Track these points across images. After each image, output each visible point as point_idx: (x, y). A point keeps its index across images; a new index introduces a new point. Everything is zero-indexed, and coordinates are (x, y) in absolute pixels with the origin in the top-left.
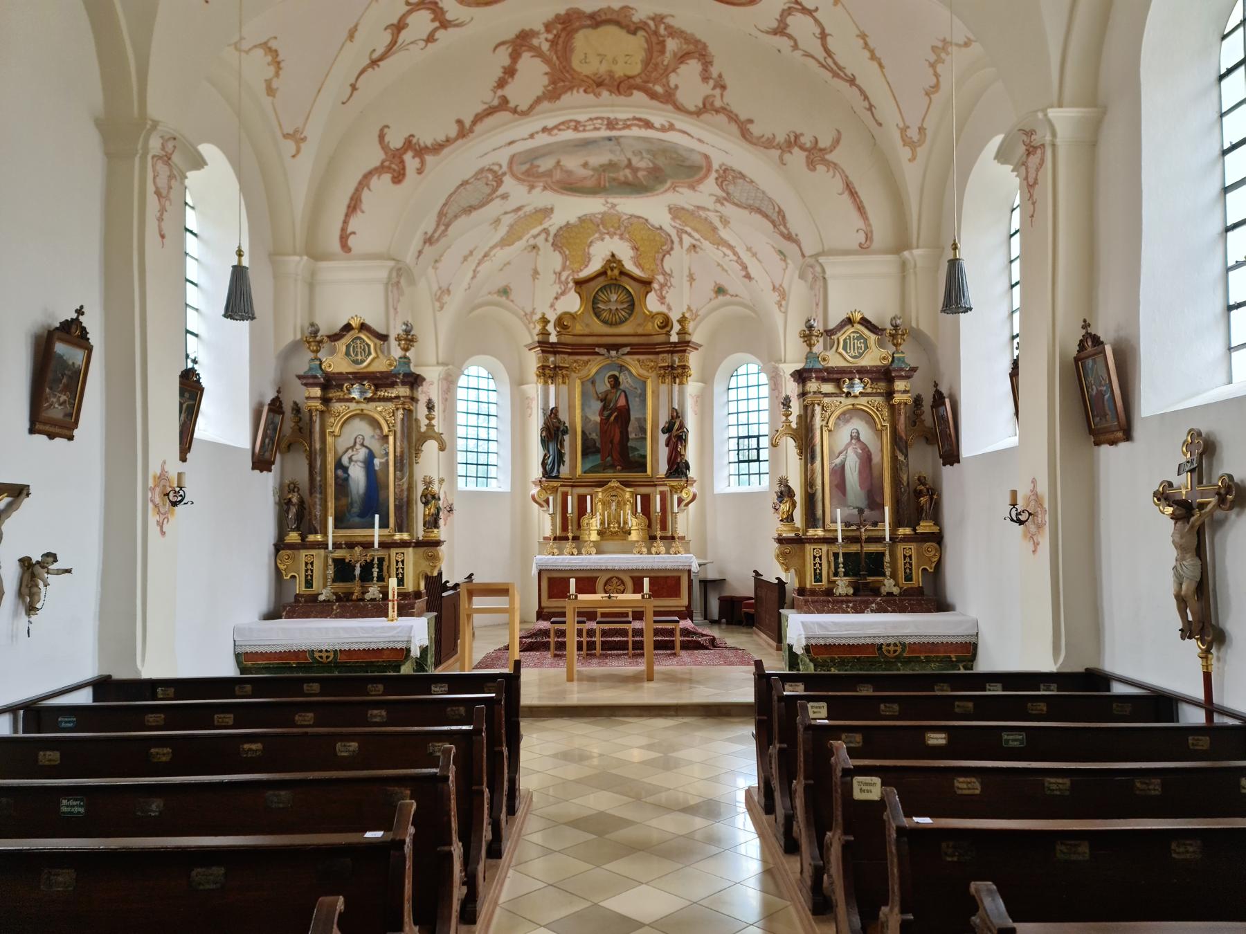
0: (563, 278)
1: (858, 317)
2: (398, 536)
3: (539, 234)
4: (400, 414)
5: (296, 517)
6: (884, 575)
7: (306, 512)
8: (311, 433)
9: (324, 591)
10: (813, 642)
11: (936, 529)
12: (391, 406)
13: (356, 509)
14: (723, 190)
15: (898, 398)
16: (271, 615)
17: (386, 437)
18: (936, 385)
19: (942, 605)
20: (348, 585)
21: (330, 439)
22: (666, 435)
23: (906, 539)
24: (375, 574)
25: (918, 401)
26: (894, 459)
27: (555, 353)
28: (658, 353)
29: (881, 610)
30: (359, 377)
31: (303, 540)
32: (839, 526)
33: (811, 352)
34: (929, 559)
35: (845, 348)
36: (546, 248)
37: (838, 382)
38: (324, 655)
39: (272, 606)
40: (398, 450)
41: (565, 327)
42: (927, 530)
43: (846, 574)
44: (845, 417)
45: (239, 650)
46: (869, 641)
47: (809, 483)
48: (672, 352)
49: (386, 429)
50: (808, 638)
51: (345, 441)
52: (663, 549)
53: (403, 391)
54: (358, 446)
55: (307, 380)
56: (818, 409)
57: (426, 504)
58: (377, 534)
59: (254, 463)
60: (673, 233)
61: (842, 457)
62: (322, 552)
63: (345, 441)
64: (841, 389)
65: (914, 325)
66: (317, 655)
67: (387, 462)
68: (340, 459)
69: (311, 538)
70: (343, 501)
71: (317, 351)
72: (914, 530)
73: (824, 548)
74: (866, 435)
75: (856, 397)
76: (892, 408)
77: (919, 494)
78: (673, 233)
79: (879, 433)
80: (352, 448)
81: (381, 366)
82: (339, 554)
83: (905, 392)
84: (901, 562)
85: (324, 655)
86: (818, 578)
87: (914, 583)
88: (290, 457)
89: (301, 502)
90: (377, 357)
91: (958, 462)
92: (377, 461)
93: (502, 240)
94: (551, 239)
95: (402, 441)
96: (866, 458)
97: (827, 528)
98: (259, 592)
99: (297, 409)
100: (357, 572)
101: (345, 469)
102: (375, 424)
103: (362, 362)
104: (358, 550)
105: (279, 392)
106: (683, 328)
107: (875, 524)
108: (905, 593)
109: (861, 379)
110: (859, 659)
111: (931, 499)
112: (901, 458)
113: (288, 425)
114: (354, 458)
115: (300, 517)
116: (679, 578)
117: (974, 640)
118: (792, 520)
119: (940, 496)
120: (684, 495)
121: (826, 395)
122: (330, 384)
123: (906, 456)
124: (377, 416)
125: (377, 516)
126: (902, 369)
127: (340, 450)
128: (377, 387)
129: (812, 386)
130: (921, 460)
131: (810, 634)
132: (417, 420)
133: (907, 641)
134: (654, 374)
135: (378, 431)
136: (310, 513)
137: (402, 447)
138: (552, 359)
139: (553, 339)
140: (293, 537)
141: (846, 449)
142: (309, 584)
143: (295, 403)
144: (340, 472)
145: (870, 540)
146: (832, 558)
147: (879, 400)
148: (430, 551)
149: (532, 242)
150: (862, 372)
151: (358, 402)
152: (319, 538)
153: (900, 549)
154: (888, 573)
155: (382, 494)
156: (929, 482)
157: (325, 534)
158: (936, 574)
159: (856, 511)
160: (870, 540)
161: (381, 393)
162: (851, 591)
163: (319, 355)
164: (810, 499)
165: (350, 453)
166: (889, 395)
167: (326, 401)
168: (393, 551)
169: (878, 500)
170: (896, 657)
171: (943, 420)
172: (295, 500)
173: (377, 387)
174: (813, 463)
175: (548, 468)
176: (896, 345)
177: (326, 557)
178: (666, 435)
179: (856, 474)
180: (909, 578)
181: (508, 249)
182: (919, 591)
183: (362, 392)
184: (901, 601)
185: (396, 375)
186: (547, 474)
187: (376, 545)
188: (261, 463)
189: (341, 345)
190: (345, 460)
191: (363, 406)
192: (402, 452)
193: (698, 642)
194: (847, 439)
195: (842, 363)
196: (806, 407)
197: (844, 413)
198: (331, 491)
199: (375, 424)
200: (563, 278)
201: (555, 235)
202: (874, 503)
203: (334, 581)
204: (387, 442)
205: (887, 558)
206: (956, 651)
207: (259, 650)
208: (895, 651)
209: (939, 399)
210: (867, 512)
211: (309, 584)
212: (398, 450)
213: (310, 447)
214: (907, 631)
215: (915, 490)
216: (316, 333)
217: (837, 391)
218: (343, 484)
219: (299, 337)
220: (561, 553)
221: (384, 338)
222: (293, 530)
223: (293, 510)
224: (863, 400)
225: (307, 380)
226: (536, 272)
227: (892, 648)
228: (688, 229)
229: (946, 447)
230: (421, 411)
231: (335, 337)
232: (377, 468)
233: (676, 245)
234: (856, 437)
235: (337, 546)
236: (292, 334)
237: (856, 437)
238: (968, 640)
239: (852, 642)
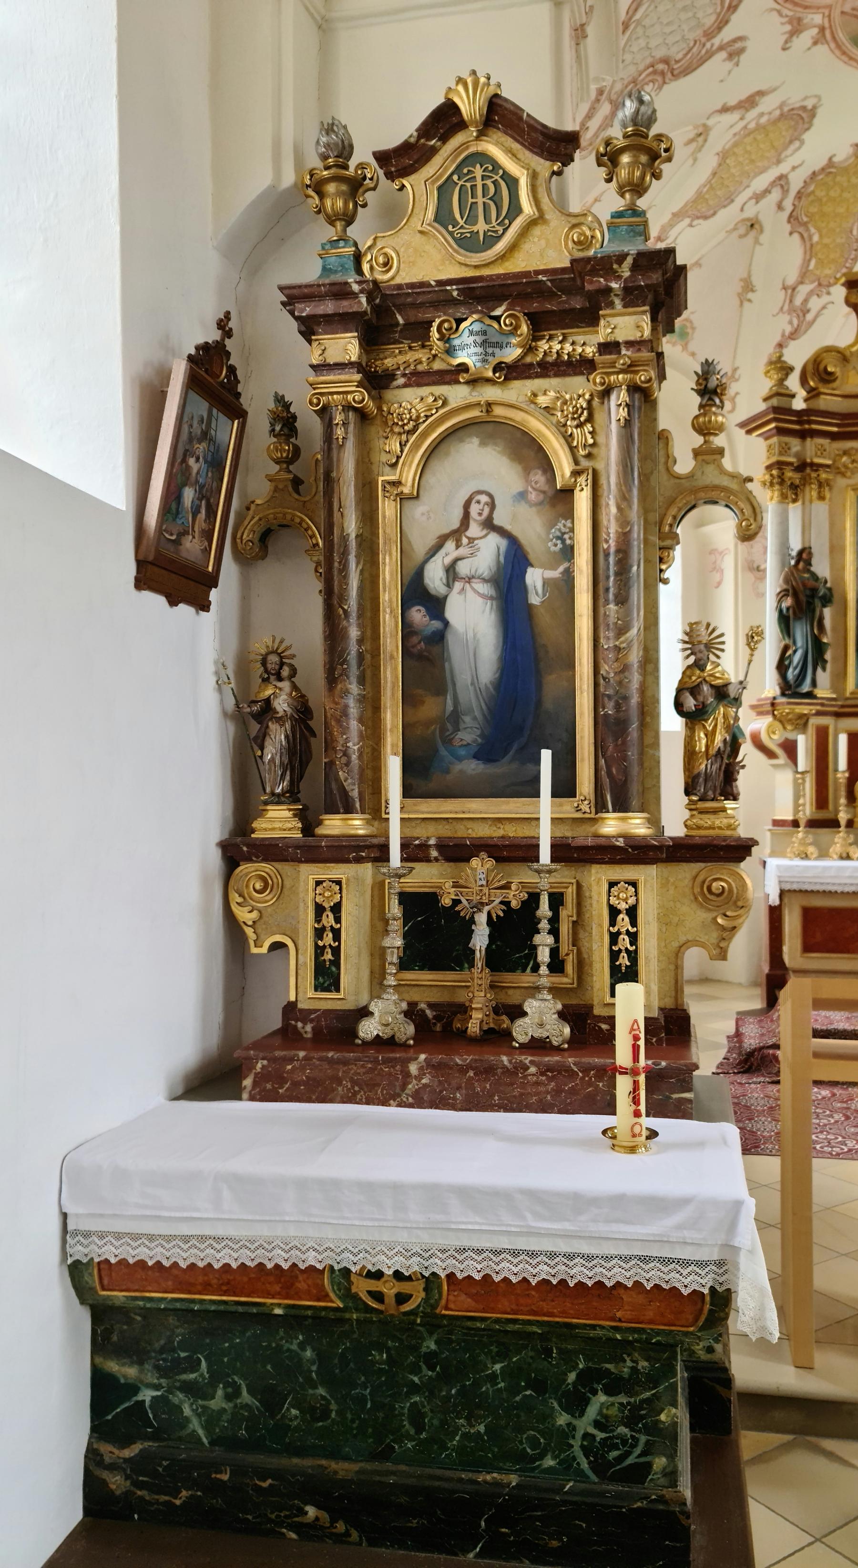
0: (798, 301)
1: (470, 107)
2: (612, 825)
3: (767, 191)
4: (617, 408)
5: (286, 758)
7: (317, 744)
8: (330, 482)
9: (376, 1007)
12: (579, 387)
13: (469, 734)
16: (212, 1080)
17: (567, 494)
20: (447, 978)
21: (387, 509)
24: (544, 955)
27: (803, 435)
30: (480, 294)
31: (308, 829)
36: (775, 223)
38: (390, 1290)
39: (214, 1040)
40: (611, 528)
41: (827, 377)
45: (78, 1252)
49: (564, 466)
51: (431, 516)
53: (626, 324)
54: (474, 530)
55: (312, 310)
57: (694, 717)
58: (545, 816)
59: (141, 564)
62: (366, 870)
63: (431, 516)
66: (361, 1287)
67: (569, 578)
68: (419, 573)
69: (334, 825)
70: (430, 708)
71: (349, 220)
80: (456, 534)
81: (546, 252)
82: (427, 876)
85: (390, 1290)
88: (269, 573)
89: (303, 712)
90: (538, 220)
92: (534, 577)
93: (699, 197)
94: (788, 205)
95: (624, 498)
98: (171, 1005)
99: (285, 421)
100: (480, 939)
101: (436, 606)
102: (528, 452)
103: (491, 239)
104: (480, 867)
105: (223, 325)
113: (257, 477)
114: (463, 568)
115: (298, 757)
122: (388, 319)
124: (536, 425)
125: (546, 756)
127: (420, 545)
128: (540, 324)
132: (664, 437)
135: (538, 477)
136: (329, 745)
137: (623, 520)
138: (795, 444)
139: (799, 404)
140: (278, 822)
142: (327, 975)
143: (279, 399)
144: (418, 615)
148: (721, 876)
149: (750, 212)
151: (474, 382)
152: (357, 825)
155: (552, 683)
157: (376, 810)
161: (551, 346)
163: (353, 231)
165: (450, 550)
167: (377, 381)
168: (598, 877)
172: (282, 705)
173: (540, 324)
175: (791, 674)
177: (379, 888)
181: (704, 226)
183: (487, 344)
185: (605, 265)
186: (789, 689)
187: (545, 855)
188: (170, 572)
189: (420, 187)
190: (434, 577)
191: (490, 393)
192: (624, 538)
198: (392, 673)
199: (528, 452)
200: (798, 301)
201: (799, 195)
203: (404, 965)
204: (569, 514)
207: (151, 1254)
208: (401, 1299)
211: (327, 975)
212: (611, 528)
213: (328, 534)
216: (345, 150)
218: (427, 653)
219: (289, 178)
220: (823, 854)
221: (558, 146)
222: (277, 799)
223: (278, 737)
225: (312, 310)
226: (748, 286)
230: (676, 402)
231: (400, 161)
232: (535, 600)
235: (414, 852)
236: (271, 162)
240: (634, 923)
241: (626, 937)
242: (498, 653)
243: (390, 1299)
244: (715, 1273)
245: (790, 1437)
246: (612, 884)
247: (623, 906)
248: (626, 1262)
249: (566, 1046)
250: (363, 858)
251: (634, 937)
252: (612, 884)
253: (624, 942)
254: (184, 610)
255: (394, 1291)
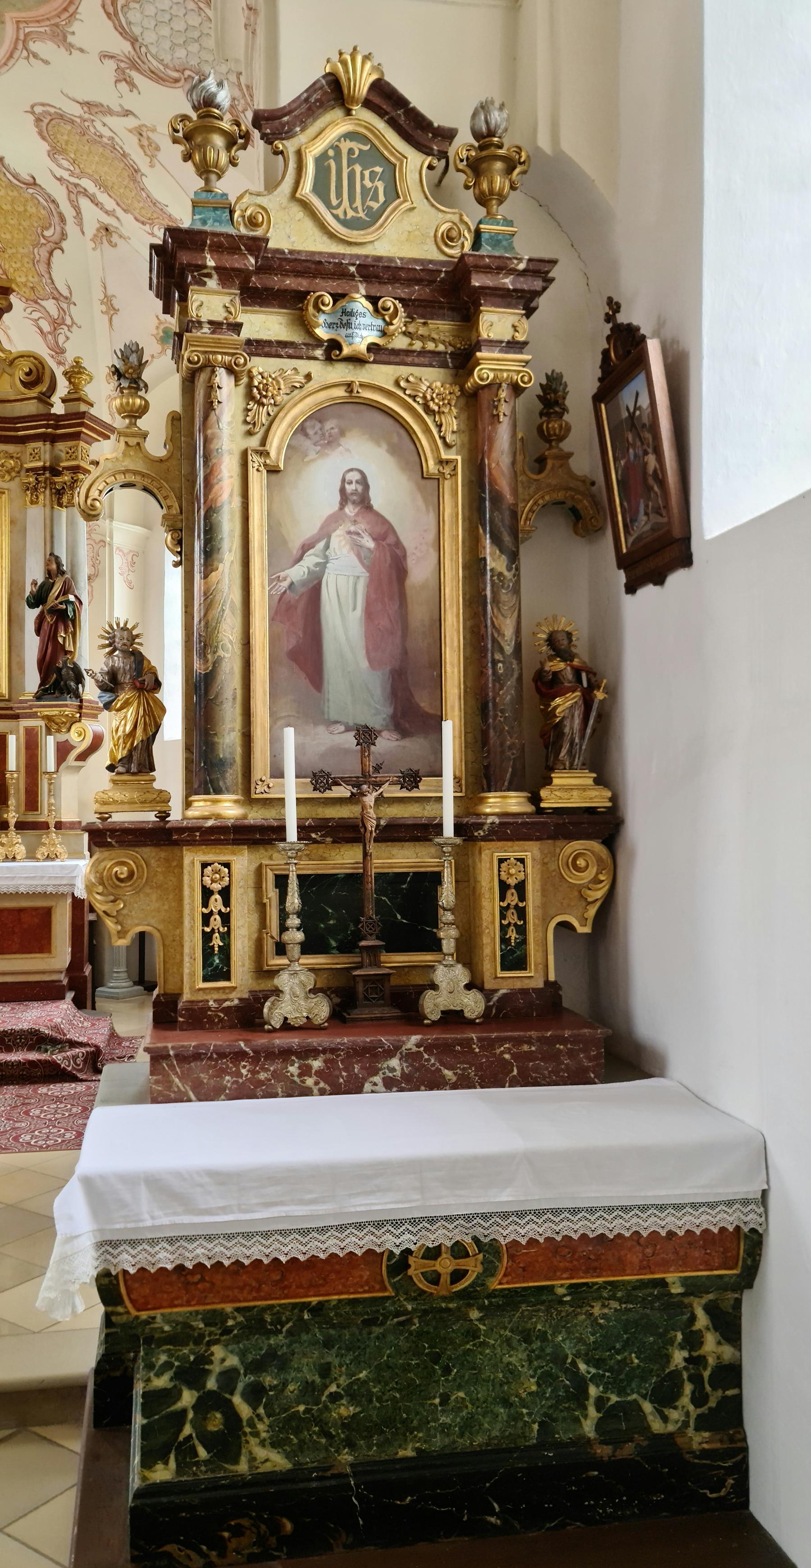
1: (362, 82)
6: (435, 945)
10: (127, 1262)
11: (599, 798)
14: (124, 33)
15: (490, 366)
18: (614, 306)
19: (621, 1057)
22: (37, 611)
23: (509, 830)
25: (552, 396)
26: (475, 567)
28: (24, 440)
29: (420, 1079)
32: (291, 789)
33: (208, 190)
34: (580, 892)
35: (321, 188)
37: (294, 302)
42: (575, 801)
43: (307, 948)
44: (320, 429)
46: (356, 1244)
47: (200, 641)
48: (53, 439)
50: (108, 1245)
52: (21, 850)
56: (229, 394)
60: (59, 193)
61: (310, 560)
64: (306, 326)
65: (544, 142)
72: (535, 799)
73: (243, 862)
74: (391, 491)
75: (356, 360)
76: (475, 403)
77: (548, 686)
78: (59, 193)
79: (429, 483)
83: (514, 346)
84: (490, 906)
86: (217, 967)
87: (531, 978)
91: (686, 560)
96: (390, 569)
97: (259, 791)
106: (75, 387)
107: (411, 779)
108: (505, 1012)
109: (373, 300)
110: (317, 1310)
111: (588, 702)
112: (495, 561)
116: (45, 916)
117: (752, 1220)
118: (148, 766)
119: (613, 692)
120: (73, 736)
121: (260, 347)
123: (514, 557)
126: (502, 267)
129: (210, 302)
130: (561, 582)
131: (119, 1227)
133: (505, 1234)
134: (14, 485)
141: (325, 533)
145: (394, 833)
146: (272, 893)
147: (432, 379)
150: (377, 274)
153: (488, 860)
154: (448, 945)
156: (581, 648)
158: (598, 941)
159: (349, 740)
160: (394, 833)
162: (322, 1009)
164: (201, 691)
166: (462, 360)
169: (424, 702)
170: (464, 1295)
171: (641, 428)
174: (209, 567)
176: (483, 200)
178: (37, 611)
179: (356, 617)
180: (514, 959)
182: (547, 1004)
184: (488, 1045)
187: (292, 834)
193: (53, 1065)
194: (330, 502)
195: (310, 242)
196: (189, 382)
197: (319, 415)
202: (414, 717)
205: (447, 894)
206: (685, 1265)
208: (458, 1275)
209: (624, 351)
210: (386, 744)
214: (505, 1197)
215: (539, 676)
217: (296, 337)
224: (382, 374)
227: (445, 1265)
228: (87, 184)
229: (643, 524)
233: (71, 228)
234: (357, 496)
237: (357, 496)
238: (729, 1219)
239: (288, 1250)
240: (227, 903)
241: (218, 917)
242: (363, 629)
243: (445, 1279)
244: (462, 1226)
245: (14, 1430)
246: (204, 865)
247: (216, 887)
248: (486, 1221)
249: (326, 1024)
250: (221, 840)
251: (226, 918)
252: (204, 865)
253: (216, 922)
254: (677, 579)
255: (451, 1269)
